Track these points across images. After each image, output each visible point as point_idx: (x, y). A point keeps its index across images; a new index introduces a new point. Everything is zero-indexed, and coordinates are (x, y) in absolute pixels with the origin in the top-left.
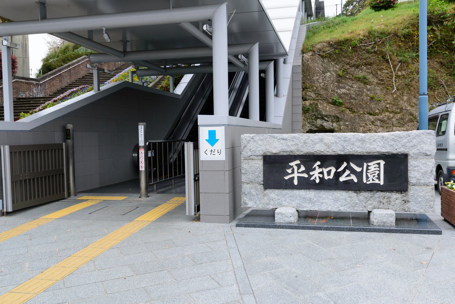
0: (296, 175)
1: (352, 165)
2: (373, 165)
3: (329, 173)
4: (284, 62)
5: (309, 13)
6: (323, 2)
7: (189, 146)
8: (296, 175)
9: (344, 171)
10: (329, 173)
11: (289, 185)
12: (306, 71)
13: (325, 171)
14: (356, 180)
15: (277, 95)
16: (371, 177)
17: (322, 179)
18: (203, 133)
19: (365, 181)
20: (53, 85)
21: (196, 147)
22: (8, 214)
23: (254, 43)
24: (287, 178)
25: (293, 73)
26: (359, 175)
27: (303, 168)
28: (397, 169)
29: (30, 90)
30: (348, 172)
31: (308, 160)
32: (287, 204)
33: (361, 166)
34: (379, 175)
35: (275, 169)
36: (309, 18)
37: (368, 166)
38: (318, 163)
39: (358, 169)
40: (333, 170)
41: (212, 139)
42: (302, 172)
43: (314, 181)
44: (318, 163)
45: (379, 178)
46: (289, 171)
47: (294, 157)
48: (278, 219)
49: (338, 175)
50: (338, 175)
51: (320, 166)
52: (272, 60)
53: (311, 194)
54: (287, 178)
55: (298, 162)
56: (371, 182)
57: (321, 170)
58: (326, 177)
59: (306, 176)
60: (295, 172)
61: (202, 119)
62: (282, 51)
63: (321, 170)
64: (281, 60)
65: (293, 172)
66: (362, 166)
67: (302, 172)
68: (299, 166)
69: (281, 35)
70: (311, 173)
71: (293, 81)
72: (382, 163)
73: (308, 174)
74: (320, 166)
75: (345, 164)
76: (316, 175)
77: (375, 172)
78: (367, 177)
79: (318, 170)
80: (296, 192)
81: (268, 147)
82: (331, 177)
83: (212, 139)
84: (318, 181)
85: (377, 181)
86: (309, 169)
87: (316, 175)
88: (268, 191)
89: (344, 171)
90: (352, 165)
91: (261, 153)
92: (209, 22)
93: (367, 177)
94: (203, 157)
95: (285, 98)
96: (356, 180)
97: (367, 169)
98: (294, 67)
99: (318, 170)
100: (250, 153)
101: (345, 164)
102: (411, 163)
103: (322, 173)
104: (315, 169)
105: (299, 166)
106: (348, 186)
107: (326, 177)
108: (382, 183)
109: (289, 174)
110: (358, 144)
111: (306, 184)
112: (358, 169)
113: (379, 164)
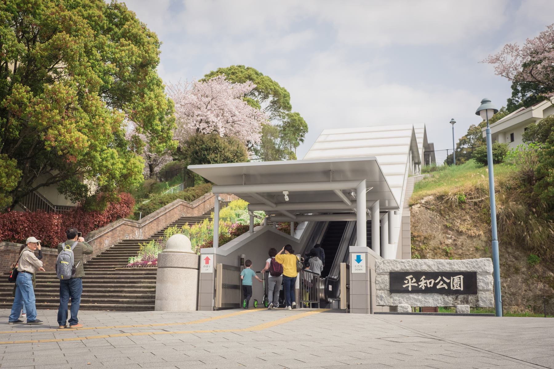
0: (410, 284)
1: (444, 278)
2: (456, 278)
3: (430, 283)
4: (395, 213)
5: (417, 161)
6: (433, 144)
7: (343, 265)
8: (410, 284)
9: (439, 282)
10: (430, 283)
11: (406, 291)
12: (415, 222)
13: (428, 282)
14: (446, 288)
15: (390, 242)
16: (455, 286)
17: (426, 287)
18: (353, 257)
19: (452, 288)
20: (152, 228)
21: (348, 267)
22: (219, 309)
23: (377, 201)
24: (404, 286)
25: (402, 223)
26: (449, 284)
27: (414, 280)
28: (470, 279)
29: (133, 232)
30: (442, 283)
31: (417, 275)
32: (405, 302)
33: (450, 279)
34: (460, 284)
35: (397, 281)
36: (417, 166)
37: (453, 279)
38: (424, 277)
39: (448, 281)
40: (433, 281)
41: (359, 260)
42: (414, 283)
43: (421, 288)
44: (424, 277)
45: (460, 286)
46: (406, 282)
47: (407, 273)
48: (400, 310)
49: (436, 284)
50: (436, 284)
51: (425, 279)
52: (387, 212)
53: (420, 297)
54: (404, 286)
55: (411, 276)
56: (456, 289)
57: (425, 281)
58: (429, 286)
59: (416, 285)
60: (410, 283)
61: (351, 248)
62: (393, 204)
63: (425, 281)
64: (392, 212)
65: (408, 283)
66: (450, 279)
67: (414, 283)
68: (412, 279)
69: (393, 190)
70: (420, 283)
71: (403, 231)
72: (462, 277)
73: (418, 284)
74: (425, 279)
75: (440, 278)
76: (422, 284)
77: (457, 283)
78: (453, 286)
79: (424, 281)
80: (412, 296)
81: (393, 267)
82: (432, 285)
83: (359, 260)
84: (423, 288)
85: (459, 288)
86: (418, 281)
87: (422, 284)
88: (393, 295)
89: (439, 282)
90: (444, 278)
91: (389, 271)
92: (356, 190)
93: (453, 286)
94: (353, 270)
95: (397, 245)
96: (446, 288)
97: (453, 281)
98: (403, 218)
99: (424, 281)
100: (381, 271)
101: (440, 278)
102: (479, 277)
103: (426, 283)
104: (422, 281)
105: (412, 279)
106: (442, 292)
107: (429, 286)
108: (462, 289)
109: (406, 284)
110: (448, 266)
111: (416, 290)
112: (448, 281)
113: (460, 278)
